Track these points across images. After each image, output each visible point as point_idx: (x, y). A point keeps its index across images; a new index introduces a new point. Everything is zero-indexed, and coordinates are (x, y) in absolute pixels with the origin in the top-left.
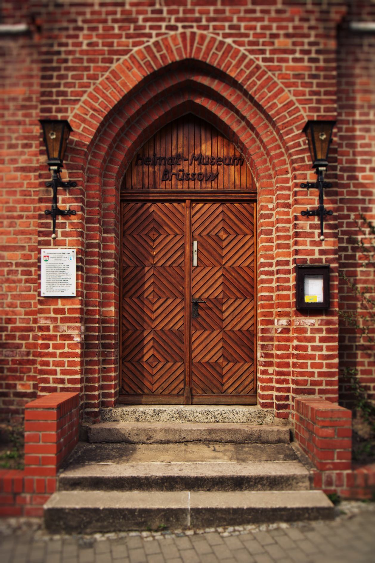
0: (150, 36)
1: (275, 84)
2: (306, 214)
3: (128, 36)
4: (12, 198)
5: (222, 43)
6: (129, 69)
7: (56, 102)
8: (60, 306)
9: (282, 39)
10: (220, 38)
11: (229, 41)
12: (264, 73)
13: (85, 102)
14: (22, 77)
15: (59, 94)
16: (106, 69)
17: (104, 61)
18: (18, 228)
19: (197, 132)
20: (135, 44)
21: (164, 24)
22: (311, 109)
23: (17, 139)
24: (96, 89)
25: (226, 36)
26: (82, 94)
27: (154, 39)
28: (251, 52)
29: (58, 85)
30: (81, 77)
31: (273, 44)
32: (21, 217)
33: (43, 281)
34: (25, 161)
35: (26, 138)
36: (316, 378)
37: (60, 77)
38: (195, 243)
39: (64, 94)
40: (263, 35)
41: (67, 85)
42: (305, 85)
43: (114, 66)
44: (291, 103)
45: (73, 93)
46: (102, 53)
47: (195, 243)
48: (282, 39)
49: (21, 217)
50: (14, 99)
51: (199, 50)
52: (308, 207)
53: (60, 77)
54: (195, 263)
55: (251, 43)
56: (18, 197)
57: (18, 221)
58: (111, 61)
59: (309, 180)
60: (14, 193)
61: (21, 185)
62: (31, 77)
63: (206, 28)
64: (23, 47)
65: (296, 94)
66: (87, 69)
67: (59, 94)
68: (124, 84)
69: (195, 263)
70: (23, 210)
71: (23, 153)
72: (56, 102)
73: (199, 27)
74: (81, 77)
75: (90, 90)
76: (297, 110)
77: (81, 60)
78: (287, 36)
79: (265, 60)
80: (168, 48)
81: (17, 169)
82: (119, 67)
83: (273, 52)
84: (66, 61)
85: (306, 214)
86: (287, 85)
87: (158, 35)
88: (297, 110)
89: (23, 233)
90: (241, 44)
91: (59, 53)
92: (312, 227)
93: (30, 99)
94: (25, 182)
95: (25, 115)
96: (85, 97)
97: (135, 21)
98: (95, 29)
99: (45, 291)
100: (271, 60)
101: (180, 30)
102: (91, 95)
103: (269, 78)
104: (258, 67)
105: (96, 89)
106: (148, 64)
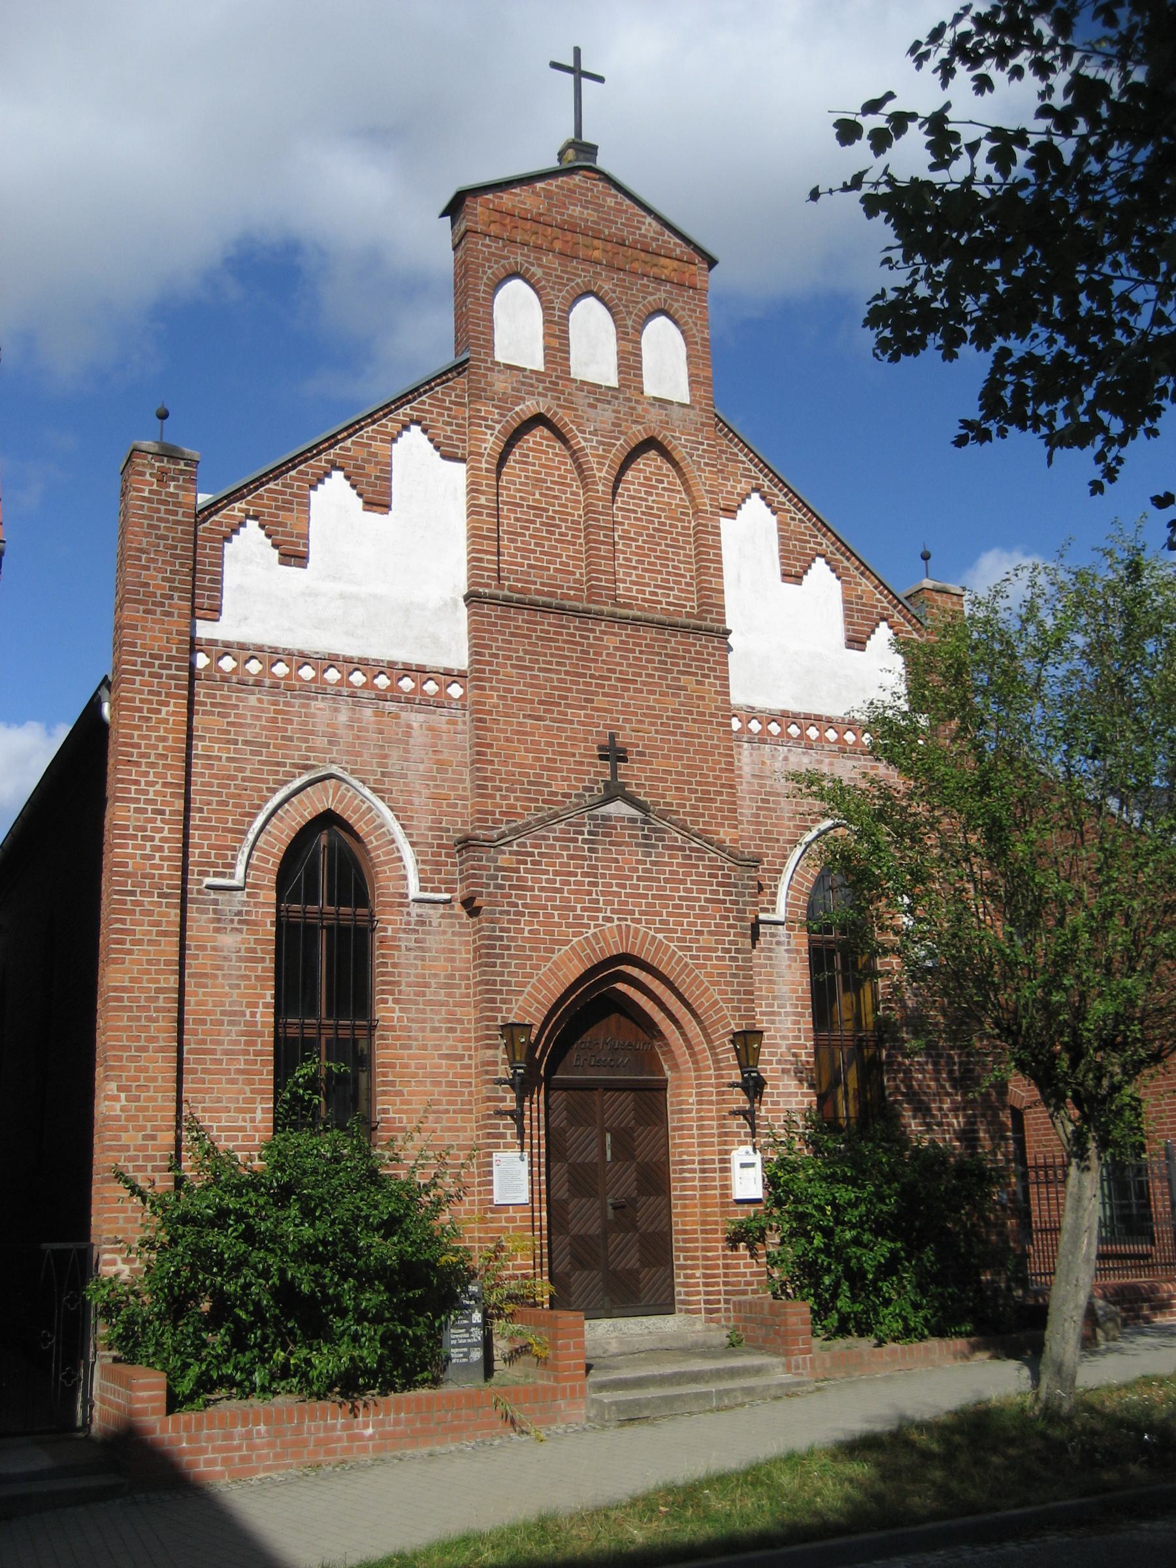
0: (588, 926)
1: (702, 982)
2: (734, 1113)
3: (568, 926)
4: (436, 1089)
5: (654, 938)
6: (570, 960)
7: (500, 992)
8: (511, 1214)
9: (706, 936)
10: (652, 933)
11: (660, 936)
12: (692, 971)
13: (529, 994)
14: (444, 951)
15: (503, 983)
16: (548, 959)
17: (546, 950)
18: (445, 1124)
19: (374, 866)
20: (575, 935)
21: (601, 915)
22: (741, 1017)
23: (440, 1021)
24: (539, 980)
25: (657, 930)
26: (524, 985)
27: (592, 931)
28: (681, 948)
29: (502, 974)
30: (524, 966)
31: (698, 941)
32: (447, 1111)
33: (496, 1187)
34: (448, 1048)
35: (449, 1021)
36: (749, 1278)
37: (504, 965)
38: (608, 1137)
39: (508, 983)
40: (689, 932)
41: (510, 974)
42: (728, 984)
43: (555, 957)
44: (716, 1002)
45: (517, 984)
46: (544, 941)
47: (608, 1137)
48: (706, 936)
49: (447, 1111)
50: (436, 976)
51: (634, 944)
52: (735, 1107)
53: (504, 965)
54: (609, 1158)
55: (680, 940)
56: (444, 1088)
57: (445, 1116)
58: (552, 951)
59: (734, 1080)
60: (439, 1084)
61: (446, 1075)
62: (453, 951)
63: (639, 921)
64: (443, 916)
65: (721, 992)
66: (530, 958)
67: (503, 983)
68: (566, 976)
69: (609, 1158)
70: (449, 1103)
71: (447, 1038)
72: (500, 992)
73: (633, 920)
74: (524, 966)
75: (534, 980)
76: (721, 1009)
77: (523, 948)
78: (711, 933)
79: (692, 957)
80: (605, 939)
81: (441, 1056)
82: (560, 957)
83: (699, 949)
84: (508, 948)
85: (734, 1113)
86: (713, 983)
87: (596, 926)
88: (721, 1009)
89: (450, 1129)
90: (671, 940)
91: (501, 938)
92: (739, 1126)
93: (452, 977)
94: (451, 1072)
95: (449, 995)
96: (528, 989)
97: (574, 909)
98: (536, 915)
99: (498, 1199)
100: (697, 958)
101: (616, 922)
102: (534, 986)
103: (697, 976)
104: (686, 965)
105: (539, 980)
106: (589, 959)
